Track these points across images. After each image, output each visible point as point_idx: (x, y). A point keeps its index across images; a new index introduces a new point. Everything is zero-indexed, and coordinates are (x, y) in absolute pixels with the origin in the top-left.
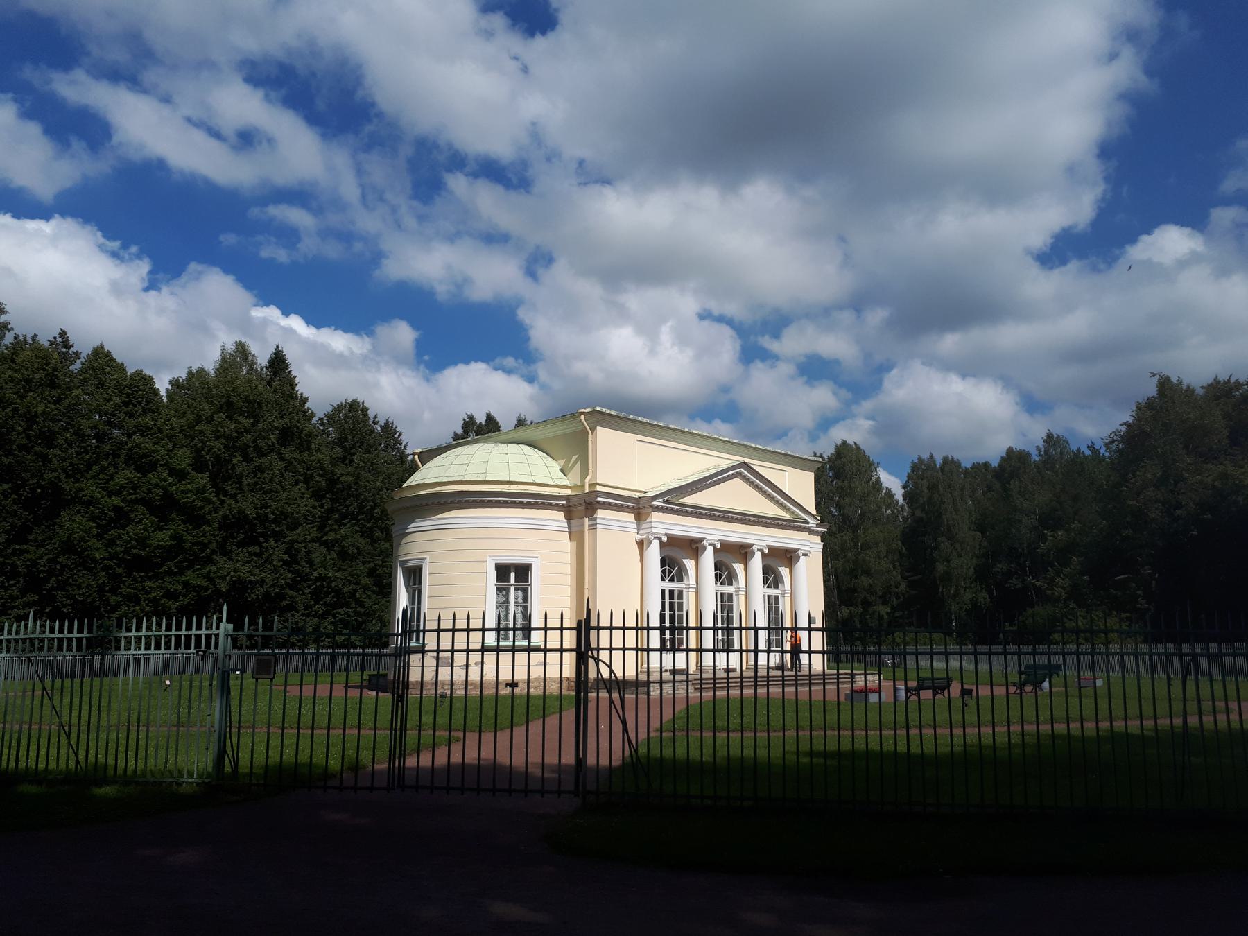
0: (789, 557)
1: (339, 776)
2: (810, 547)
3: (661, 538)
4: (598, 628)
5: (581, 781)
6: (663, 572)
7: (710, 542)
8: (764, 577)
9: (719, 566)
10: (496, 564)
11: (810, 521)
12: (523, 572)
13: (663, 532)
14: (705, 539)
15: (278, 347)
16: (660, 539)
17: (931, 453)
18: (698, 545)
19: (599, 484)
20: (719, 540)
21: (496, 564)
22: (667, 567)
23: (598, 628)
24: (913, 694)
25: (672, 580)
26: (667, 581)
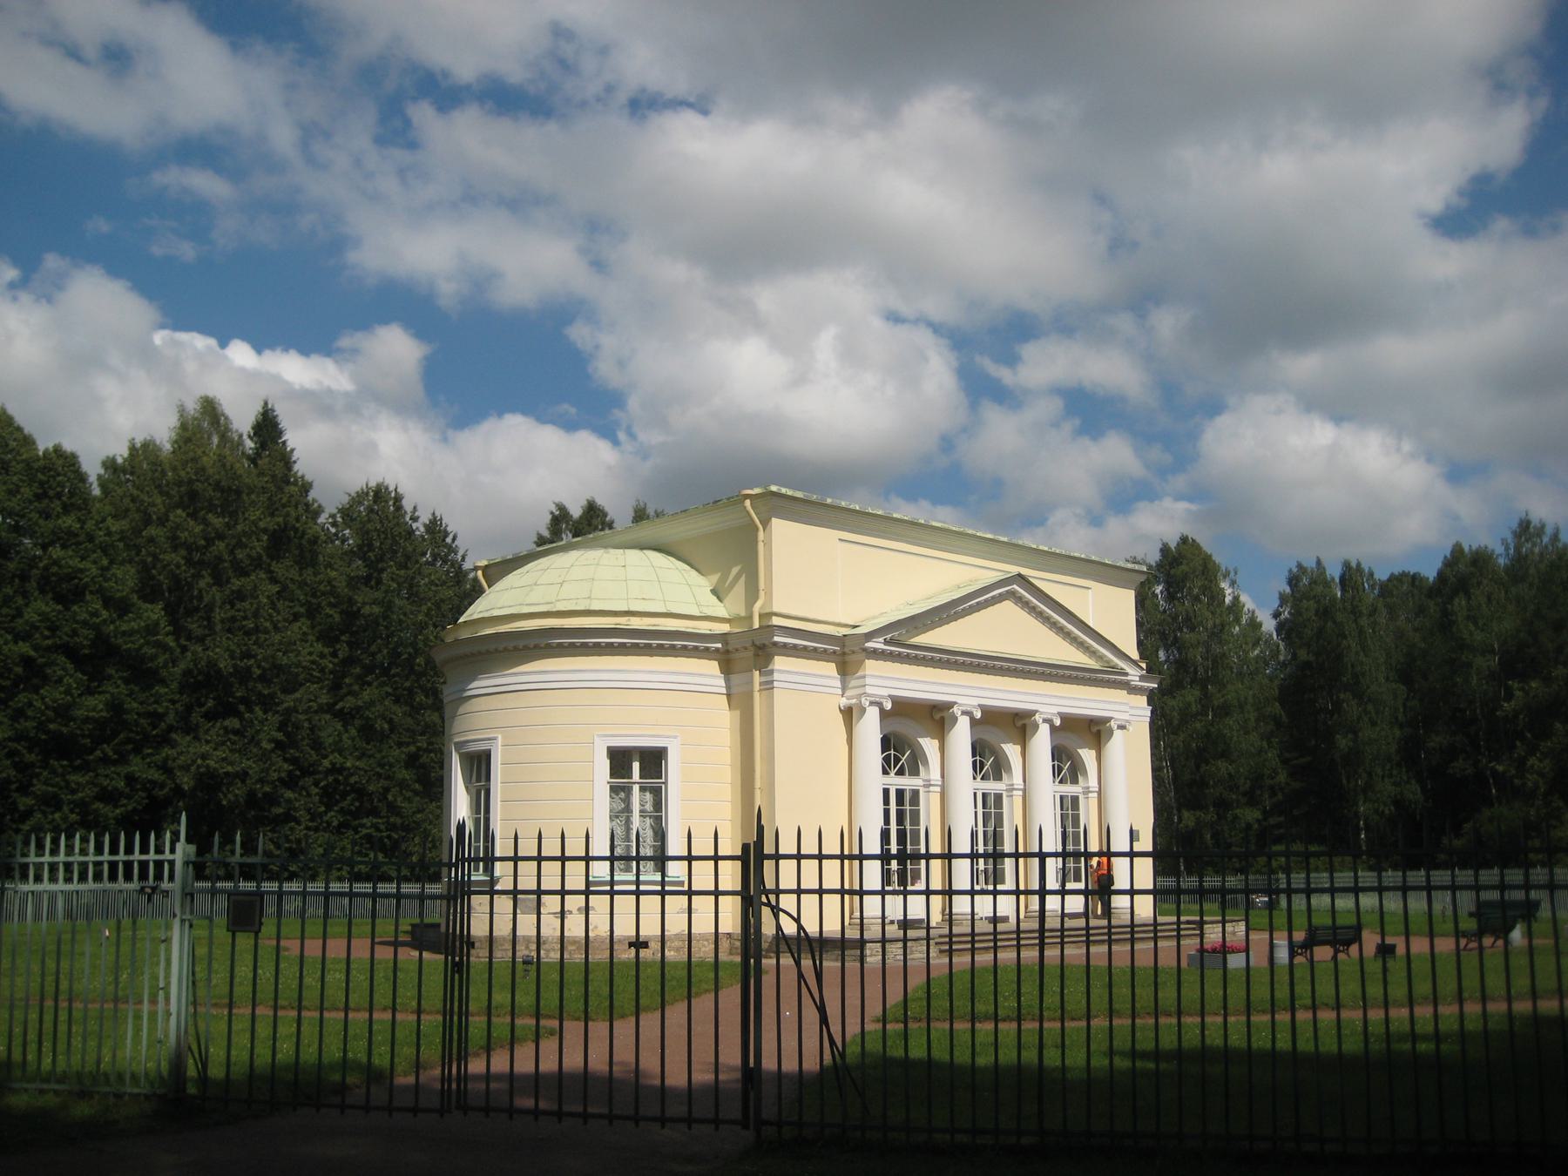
0: (1095, 731)
4: (777, 857)
6: (886, 760)
8: (1054, 766)
10: (609, 748)
12: (654, 760)
13: (885, 692)
20: (1059, 713)
23: (777, 857)
25: (900, 773)
26: (892, 774)
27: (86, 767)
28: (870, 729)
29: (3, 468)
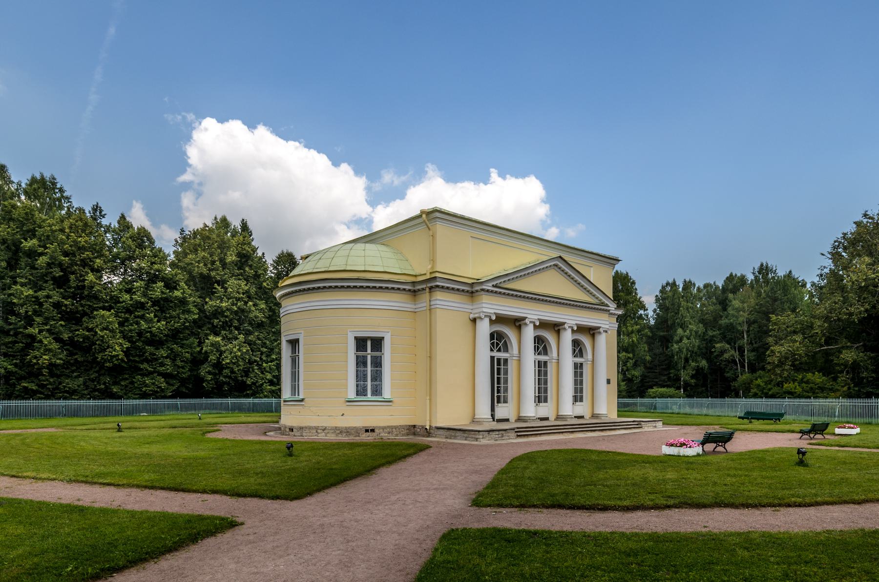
0: (592, 332)
2: (607, 323)
3: (490, 317)
6: (492, 344)
7: (531, 320)
8: (535, 346)
9: (576, 343)
10: (355, 337)
11: (610, 305)
13: (492, 311)
14: (526, 318)
16: (534, 323)
18: (558, 328)
19: (438, 272)
20: (576, 324)
25: (499, 350)
26: (495, 351)
27: (801, 323)
28: (484, 329)
29: (876, 559)
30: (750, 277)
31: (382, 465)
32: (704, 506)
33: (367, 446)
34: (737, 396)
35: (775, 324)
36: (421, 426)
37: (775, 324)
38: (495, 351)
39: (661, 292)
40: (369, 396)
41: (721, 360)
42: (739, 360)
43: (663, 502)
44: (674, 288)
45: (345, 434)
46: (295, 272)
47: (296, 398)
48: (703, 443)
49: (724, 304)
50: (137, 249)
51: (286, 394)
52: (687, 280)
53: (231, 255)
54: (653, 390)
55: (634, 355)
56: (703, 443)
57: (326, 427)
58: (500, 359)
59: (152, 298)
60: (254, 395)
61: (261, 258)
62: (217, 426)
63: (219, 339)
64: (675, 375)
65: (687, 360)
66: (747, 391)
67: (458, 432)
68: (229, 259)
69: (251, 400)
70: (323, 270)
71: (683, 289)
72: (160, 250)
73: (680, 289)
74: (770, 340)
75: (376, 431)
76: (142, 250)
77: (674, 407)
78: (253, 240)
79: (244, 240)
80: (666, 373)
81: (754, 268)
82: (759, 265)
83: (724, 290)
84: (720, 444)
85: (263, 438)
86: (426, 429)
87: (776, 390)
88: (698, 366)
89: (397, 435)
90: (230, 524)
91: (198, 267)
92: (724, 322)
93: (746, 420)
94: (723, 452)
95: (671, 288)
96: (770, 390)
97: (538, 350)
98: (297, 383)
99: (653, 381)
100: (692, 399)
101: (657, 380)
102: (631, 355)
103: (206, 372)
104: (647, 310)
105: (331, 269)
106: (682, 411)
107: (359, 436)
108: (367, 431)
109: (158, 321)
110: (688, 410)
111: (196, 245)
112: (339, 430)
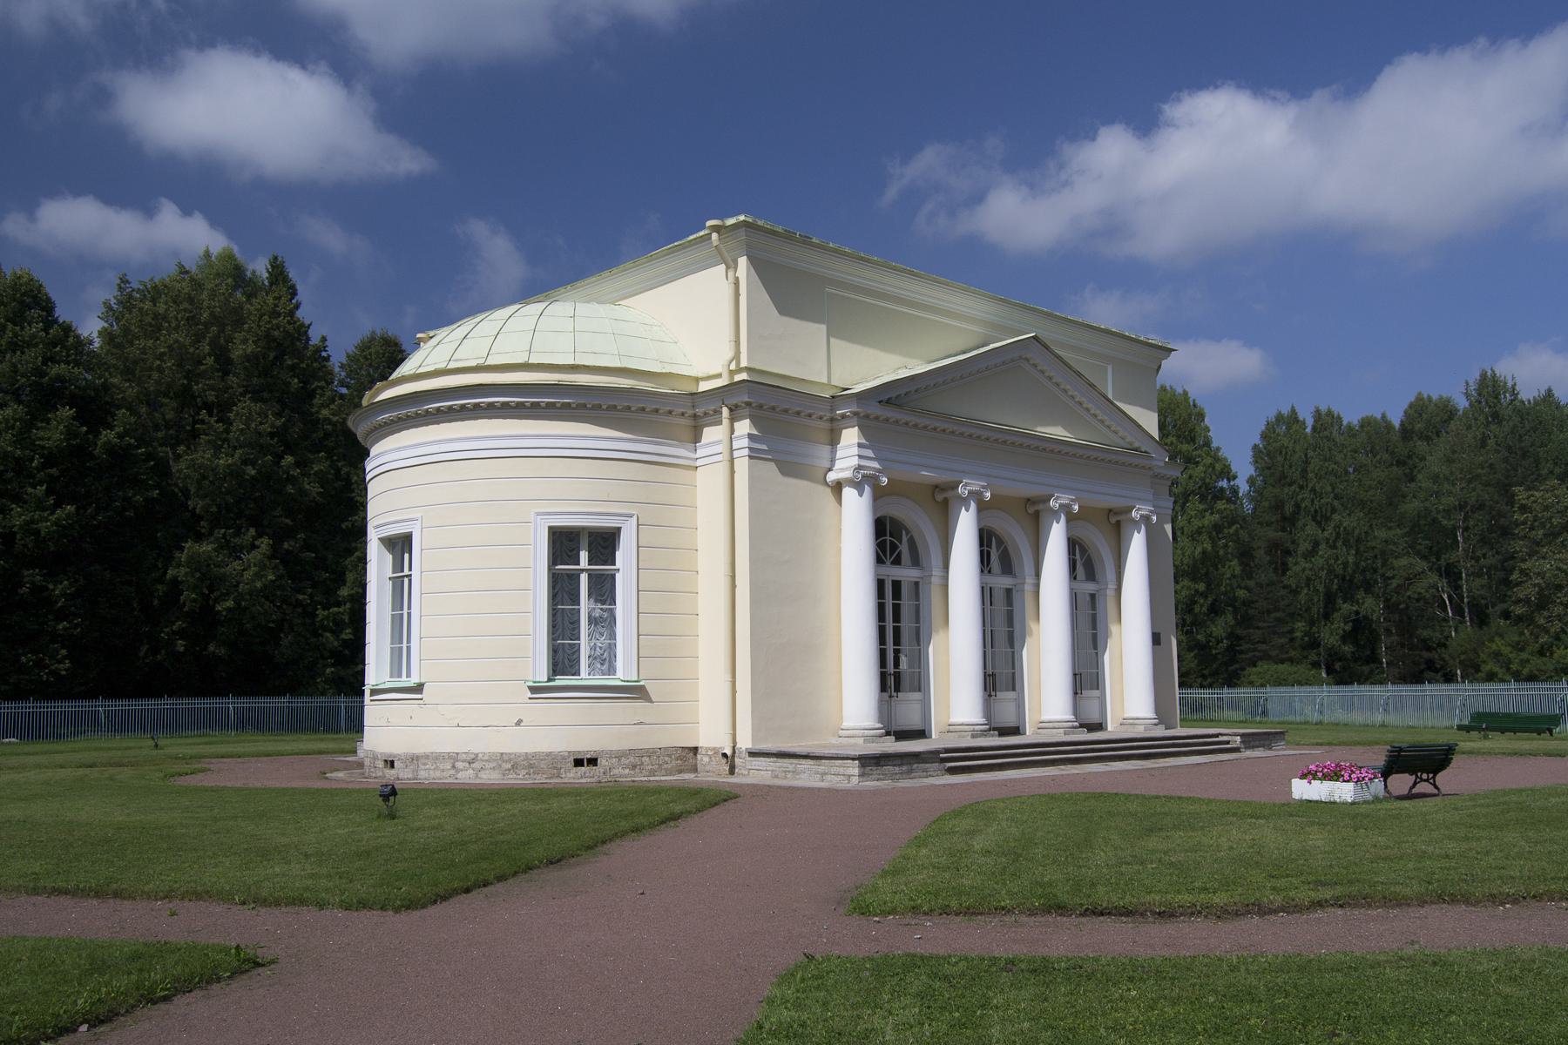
1: (589, 572)
5: (938, 318)
10: (550, 528)
12: (604, 543)
15: (276, 258)
17: (1293, 407)
21: (550, 528)
22: (888, 538)
24: (1422, 780)
26: (888, 563)
30: (1462, 403)
31: (621, 835)
32: (1399, 902)
33: (579, 794)
34: (1449, 678)
35: (1523, 509)
36: (714, 748)
37: (1523, 509)
38: (888, 563)
39: (1264, 436)
40: (585, 677)
41: (1409, 597)
42: (1450, 597)
43: (1305, 895)
44: (1295, 427)
45: (523, 772)
46: (406, 368)
47: (405, 682)
48: (1386, 774)
49: (1407, 465)
50: (10, 326)
51: (376, 671)
52: (1323, 408)
53: (245, 341)
54: (1258, 669)
55: (1208, 586)
56: (1386, 774)
57: (477, 755)
58: (899, 582)
59: (43, 447)
60: (293, 688)
61: (318, 350)
62: (200, 762)
63: (206, 547)
64: (1306, 635)
65: (1330, 599)
66: (1473, 671)
67: (803, 761)
68: (237, 352)
69: (284, 701)
70: (473, 363)
71: (1314, 429)
72: (67, 329)
73: (1308, 430)
74: (1519, 546)
75: (602, 762)
76: (22, 328)
77: (1308, 710)
78: (297, 306)
79: (276, 306)
80: (1285, 630)
81: (1467, 383)
82: (1477, 376)
83: (1406, 432)
84: (1425, 776)
85: (319, 784)
86: (725, 755)
87: (1537, 662)
88: (1357, 613)
89: (652, 773)
90: (248, 964)
91: (160, 370)
92: (1411, 507)
93: (1474, 734)
94: (1434, 795)
95: (1288, 428)
96: (1524, 662)
97: (988, 566)
98: (405, 645)
99: (1255, 650)
100: (1349, 688)
101: (1263, 647)
102: (1201, 587)
103: (174, 633)
104: (1235, 477)
105: (492, 361)
106: (1326, 719)
107: (559, 776)
108: (578, 763)
109: (58, 505)
110: (1341, 716)
111: (156, 316)
112: (510, 760)
